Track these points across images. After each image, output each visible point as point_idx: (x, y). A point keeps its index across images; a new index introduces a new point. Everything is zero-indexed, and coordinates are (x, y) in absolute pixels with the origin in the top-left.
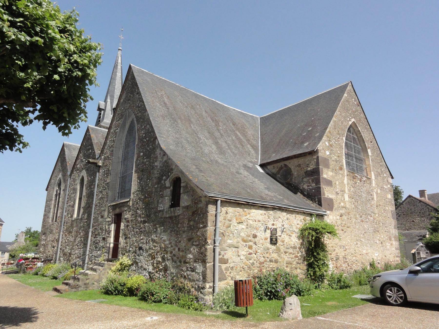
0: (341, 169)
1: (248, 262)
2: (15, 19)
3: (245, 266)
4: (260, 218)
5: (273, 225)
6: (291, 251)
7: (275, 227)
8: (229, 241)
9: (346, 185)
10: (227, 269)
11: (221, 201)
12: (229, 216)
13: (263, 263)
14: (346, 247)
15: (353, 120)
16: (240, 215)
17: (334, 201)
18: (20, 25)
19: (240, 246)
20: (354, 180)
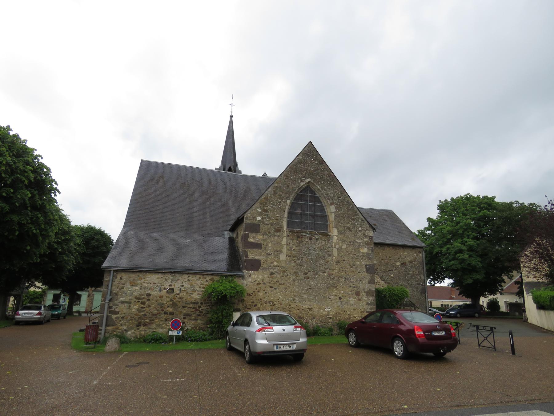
0: (279, 230)
1: (140, 314)
2: (54, 312)
3: (136, 317)
4: (156, 281)
5: (171, 285)
6: (191, 306)
7: (172, 287)
8: (121, 299)
9: (285, 246)
10: (117, 318)
11: (114, 271)
12: (122, 282)
13: (156, 315)
14: (275, 303)
15: (308, 180)
16: (134, 280)
17: (262, 263)
18: (442, 279)
19: (133, 302)
20: (299, 239)
